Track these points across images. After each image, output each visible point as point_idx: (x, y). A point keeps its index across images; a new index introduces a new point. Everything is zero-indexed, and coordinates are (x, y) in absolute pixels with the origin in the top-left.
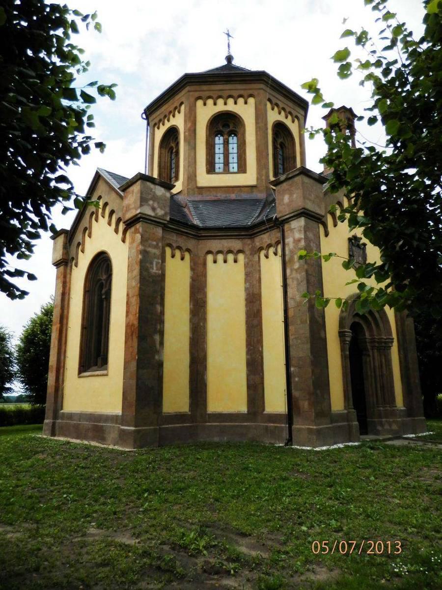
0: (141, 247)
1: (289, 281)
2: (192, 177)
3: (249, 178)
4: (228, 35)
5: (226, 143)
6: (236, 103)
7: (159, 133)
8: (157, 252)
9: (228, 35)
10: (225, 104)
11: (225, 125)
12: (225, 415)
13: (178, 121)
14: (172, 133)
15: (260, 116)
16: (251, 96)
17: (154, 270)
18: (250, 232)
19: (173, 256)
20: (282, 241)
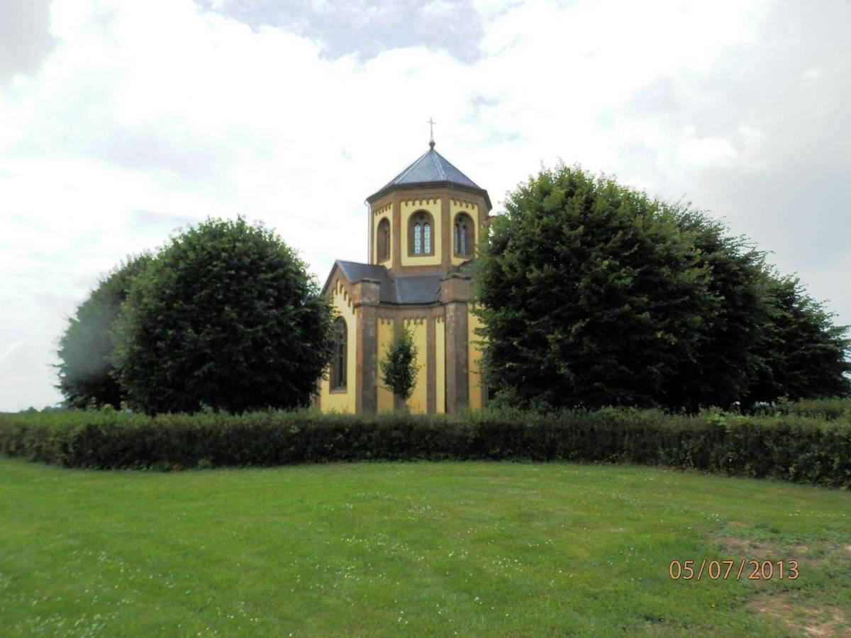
0: (363, 322)
1: (447, 340)
2: (398, 260)
3: (436, 260)
4: (431, 123)
5: (423, 232)
6: (428, 203)
7: (378, 219)
8: (372, 323)
9: (431, 123)
10: (421, 204)
11: (421, 218)
12: (569, 456)
13: (389, 214)
14: (384, 222)
15: (445, 211)
16: (438, 198)
17: (371, 334)
18: (430, 306)
19: (383, 323)
20: (444, 316)
